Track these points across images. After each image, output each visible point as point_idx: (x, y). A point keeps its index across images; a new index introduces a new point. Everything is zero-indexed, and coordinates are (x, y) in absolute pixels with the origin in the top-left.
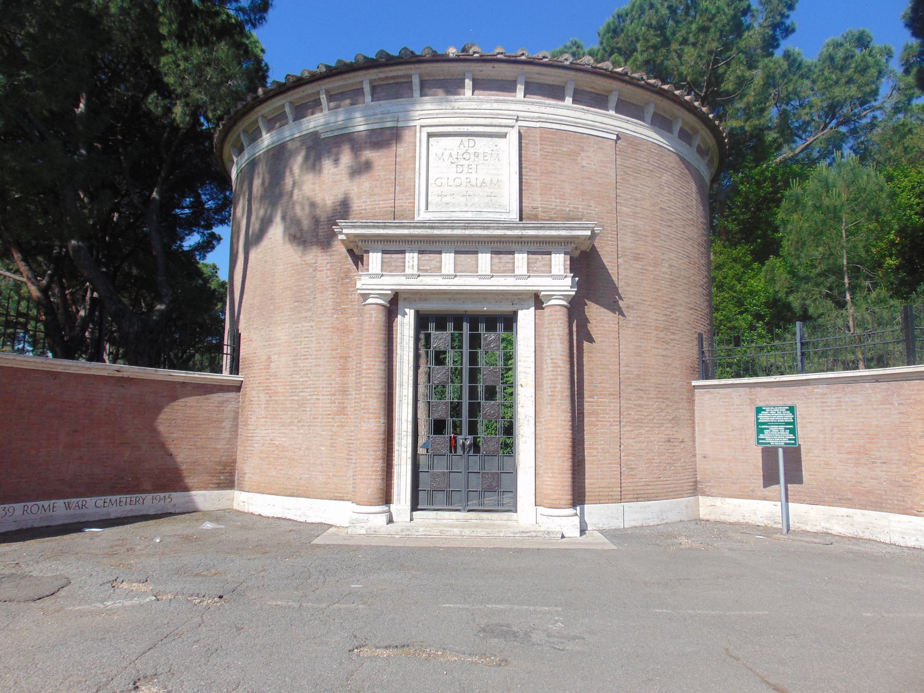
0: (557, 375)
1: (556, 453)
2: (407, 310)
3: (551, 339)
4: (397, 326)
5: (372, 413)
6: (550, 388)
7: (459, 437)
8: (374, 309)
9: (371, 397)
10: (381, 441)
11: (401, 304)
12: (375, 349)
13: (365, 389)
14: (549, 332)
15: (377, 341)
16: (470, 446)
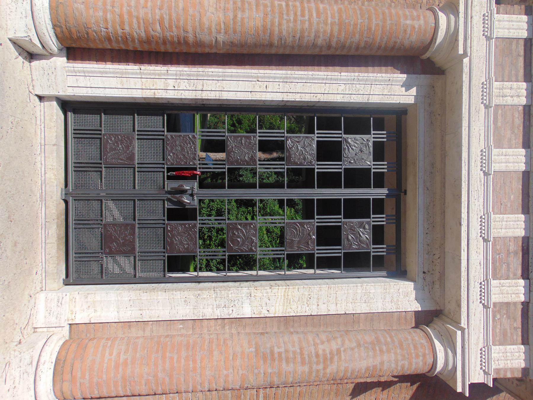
0: (310, 363)
1: (164, 370)
2: (413, 91)
3: (374, 349)
4: (386, 72)
5: (235, 16)
6: (287, 351)
7: (196, 185)
8: (426, 23)
9: (266, 14)
10: (182, 34)
11: (424, 79)
12: (355, 25)
13: (280, 6)
14: (386, 344)
15: (370, 29)
16: (181, 203)
